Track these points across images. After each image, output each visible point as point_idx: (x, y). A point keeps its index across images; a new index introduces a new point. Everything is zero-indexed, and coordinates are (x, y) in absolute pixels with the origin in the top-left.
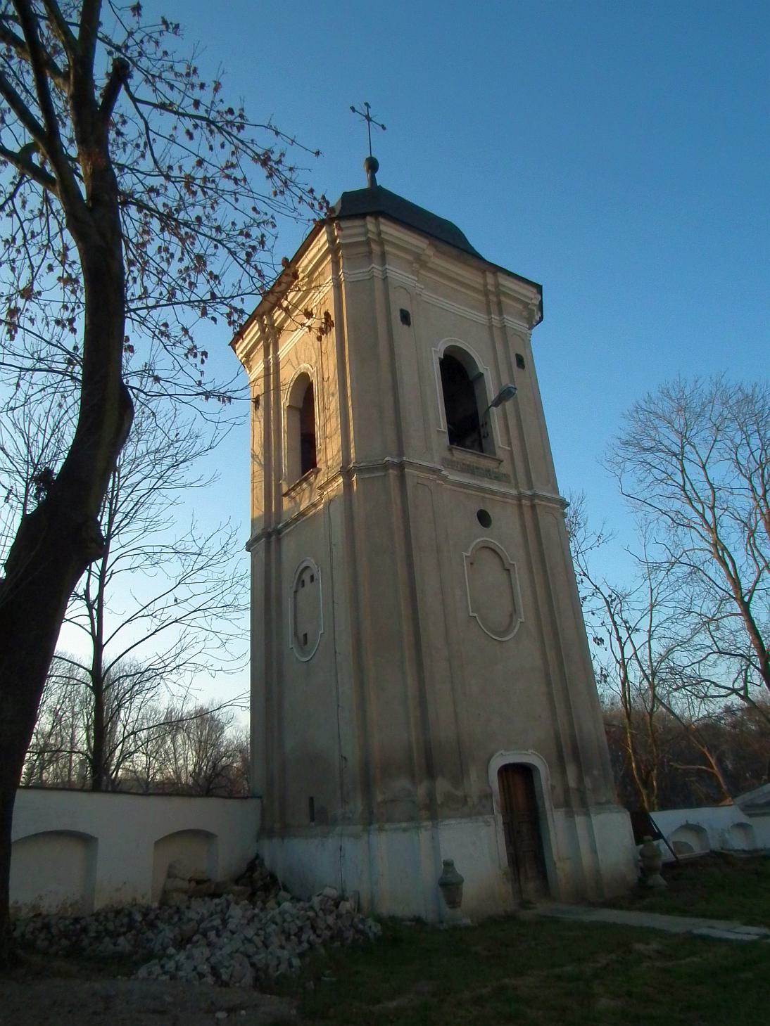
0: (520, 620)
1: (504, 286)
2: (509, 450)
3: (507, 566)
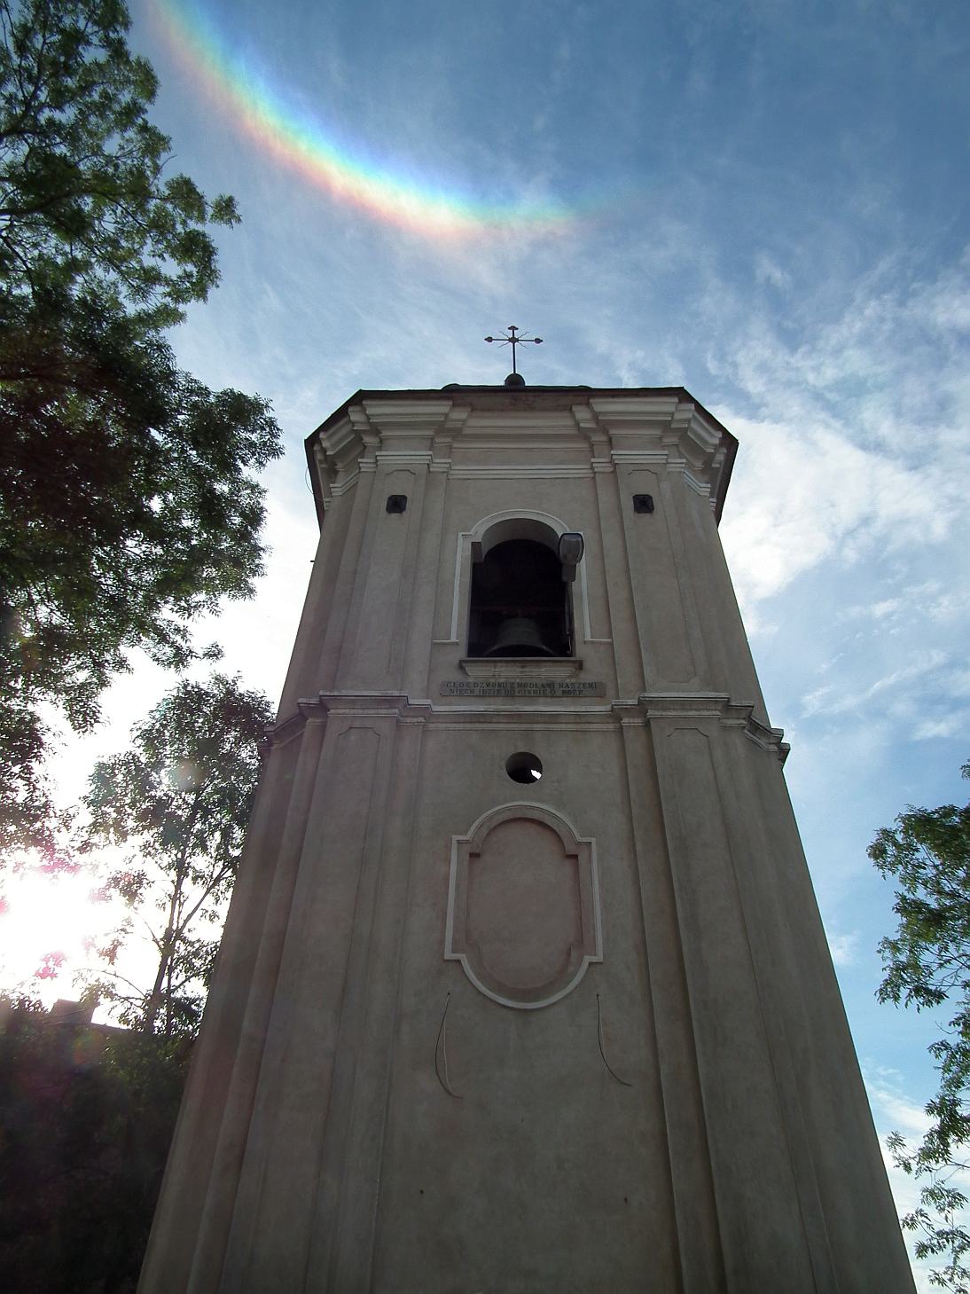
0: (587, 959)
1: (604, 413)
2: (608, 643)
3: (571, 849)
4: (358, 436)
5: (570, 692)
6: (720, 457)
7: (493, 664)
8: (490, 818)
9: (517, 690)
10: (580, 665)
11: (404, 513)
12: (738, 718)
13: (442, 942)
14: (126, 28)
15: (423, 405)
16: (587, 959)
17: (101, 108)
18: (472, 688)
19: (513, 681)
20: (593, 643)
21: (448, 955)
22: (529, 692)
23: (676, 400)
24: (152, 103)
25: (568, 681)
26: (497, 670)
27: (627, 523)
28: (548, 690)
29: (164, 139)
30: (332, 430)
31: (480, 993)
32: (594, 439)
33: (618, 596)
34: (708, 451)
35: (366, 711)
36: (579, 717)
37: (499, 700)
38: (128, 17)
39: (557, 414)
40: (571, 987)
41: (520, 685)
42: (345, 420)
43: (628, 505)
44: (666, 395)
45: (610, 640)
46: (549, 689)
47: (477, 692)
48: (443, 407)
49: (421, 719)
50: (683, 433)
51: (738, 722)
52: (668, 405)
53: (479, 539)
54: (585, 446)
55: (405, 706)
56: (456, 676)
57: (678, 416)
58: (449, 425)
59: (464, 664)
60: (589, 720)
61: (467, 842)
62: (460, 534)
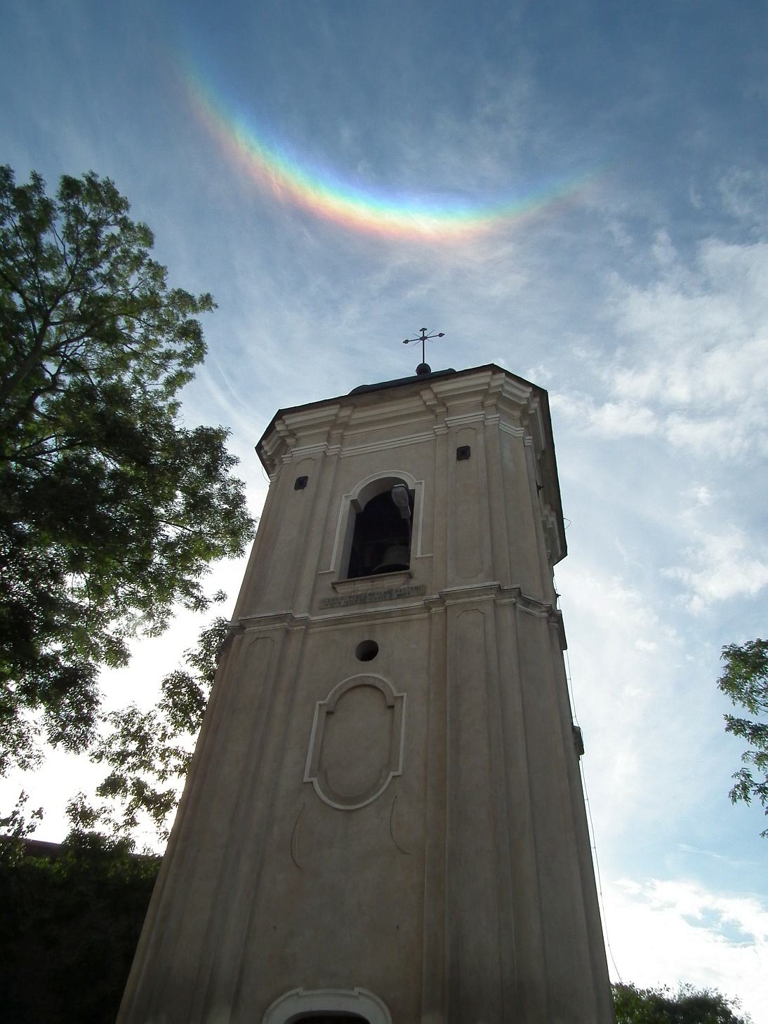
1: (441, 393)
4: (283, 439)
5: (402, 595)
6: (535, 405)
7: (370, 581)
8: (341, 688)
9: (368, 598)
10: (410, 576)
11: (305, 488)
12: (511, 598)
13: (303, 772)
14: (127, 210)
15: (324, 411)
16: (392, 774)
17: (119, 260)
20: (421, 558)
21: (306, 779)
23: (490, 373)
24: (153, 248)
25: (402, 587)
26: (356, 586)
28: (389, 595)
29: (162, 268)
30: (269, 439)
31: (323, 802)
32: (299, 435)
34: (522, 403)
36: (404, 612)
37: (356, 607)
38: (127, 202)
39: (411, 399)
40: (380, 793)
41: (370, 594)
42: (274, 431)
44: (482, 371)
47: (342, 603)
48: (333, 410)
49: (304, 627)
50: (499, 395)
51: (510, 600)
52: (484, 378)
54: (431, 417)
57: (493, 384)
58: (491, 392)
61: (325, 705)
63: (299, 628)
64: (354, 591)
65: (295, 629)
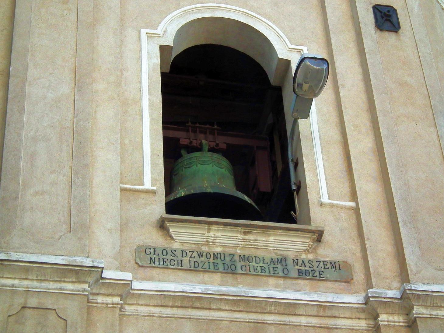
2: (351, 208)
5: (309, 272)
9: (239, 265)
10: (318, 236)
18: (180, 258)
19: (231, 251)
20: (331, 206)
22: (255, 270)
25: (304, 256)
26: (212, 234)
27: (368, 43)
28: (279, 267)
33: (361, 145)
35: (43, 284)
37: (217, 277)
41: (243, 258)
43: (367, 19)
45: (353, 204)
46: (279, 266)
49: (117, 300)
53: (169, 41)
55: (97, 281)
56: (156, 239)
59: (168, 224)
60: (337, 313)
62: (144, 31)
63: (109, 300)
64: (207, 243)
65: (100, 299)
